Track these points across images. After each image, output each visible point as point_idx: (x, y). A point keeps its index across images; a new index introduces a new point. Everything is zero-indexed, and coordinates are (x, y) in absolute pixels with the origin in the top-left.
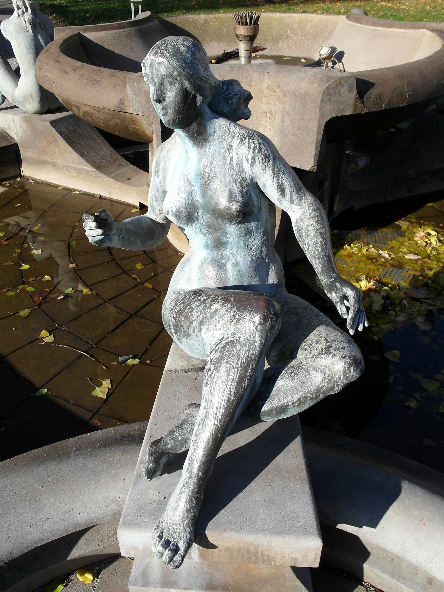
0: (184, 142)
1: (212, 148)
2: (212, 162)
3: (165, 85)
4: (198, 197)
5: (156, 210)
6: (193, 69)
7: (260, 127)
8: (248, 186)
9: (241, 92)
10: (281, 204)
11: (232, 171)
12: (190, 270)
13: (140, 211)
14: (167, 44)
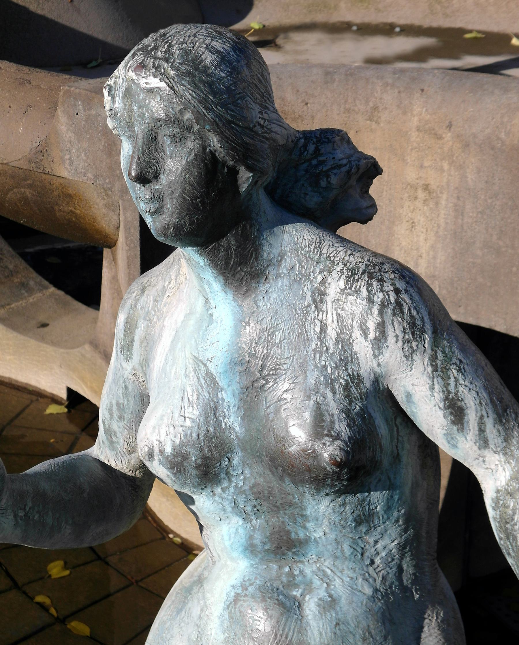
0: (201, 279)
1: (274, 295)
2: (273, 333)
3: (161, 143)
4: (231, 419)
5: (118, 442)
6: (233, 108)
7: (397, 223)
8: (365, 396)
9: (352, 159)
10: (455, 446)
11: (323, 358)
12: (202, 610)
13: (69, 411)
14: (170, 46)
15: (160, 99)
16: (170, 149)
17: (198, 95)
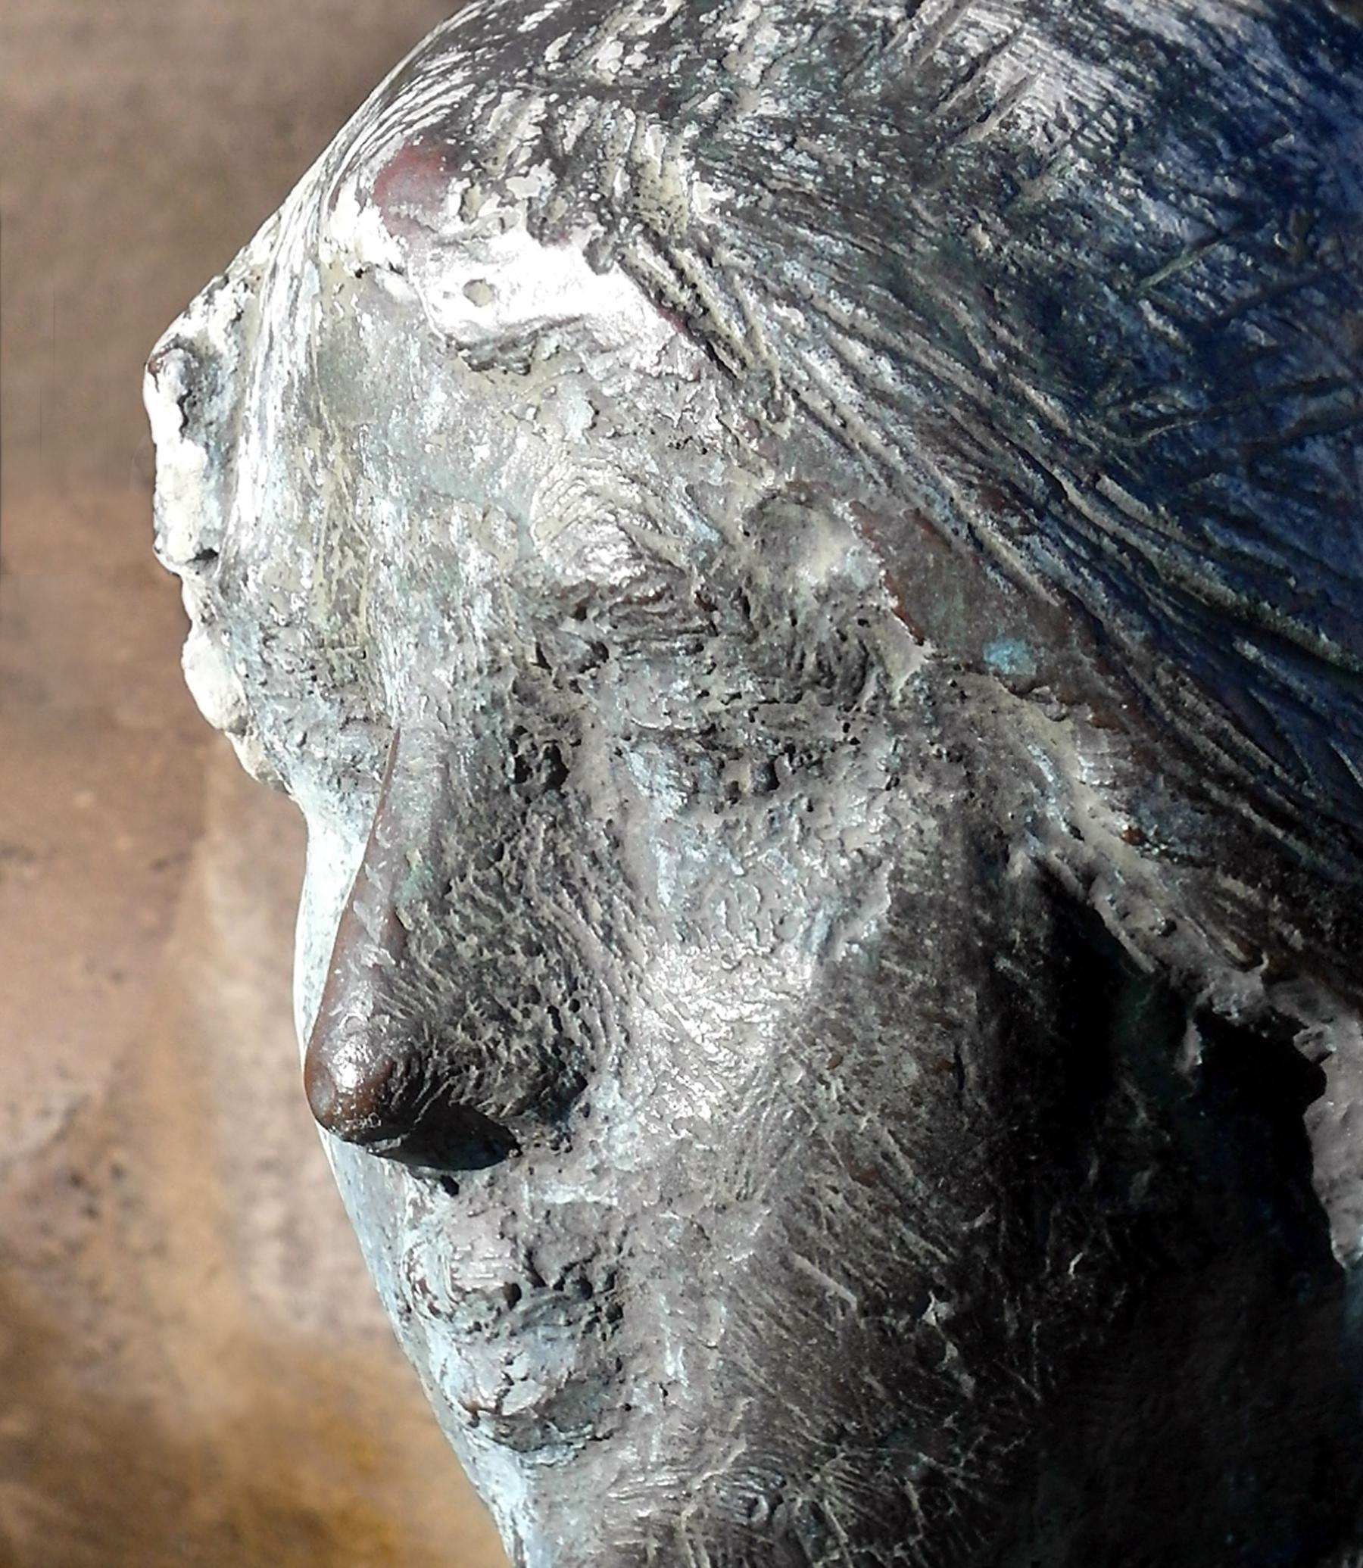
3: (605, 808)
6: (1247, 498)
15: (585, 417)
16: (683, 863)
17: (921, 376)
